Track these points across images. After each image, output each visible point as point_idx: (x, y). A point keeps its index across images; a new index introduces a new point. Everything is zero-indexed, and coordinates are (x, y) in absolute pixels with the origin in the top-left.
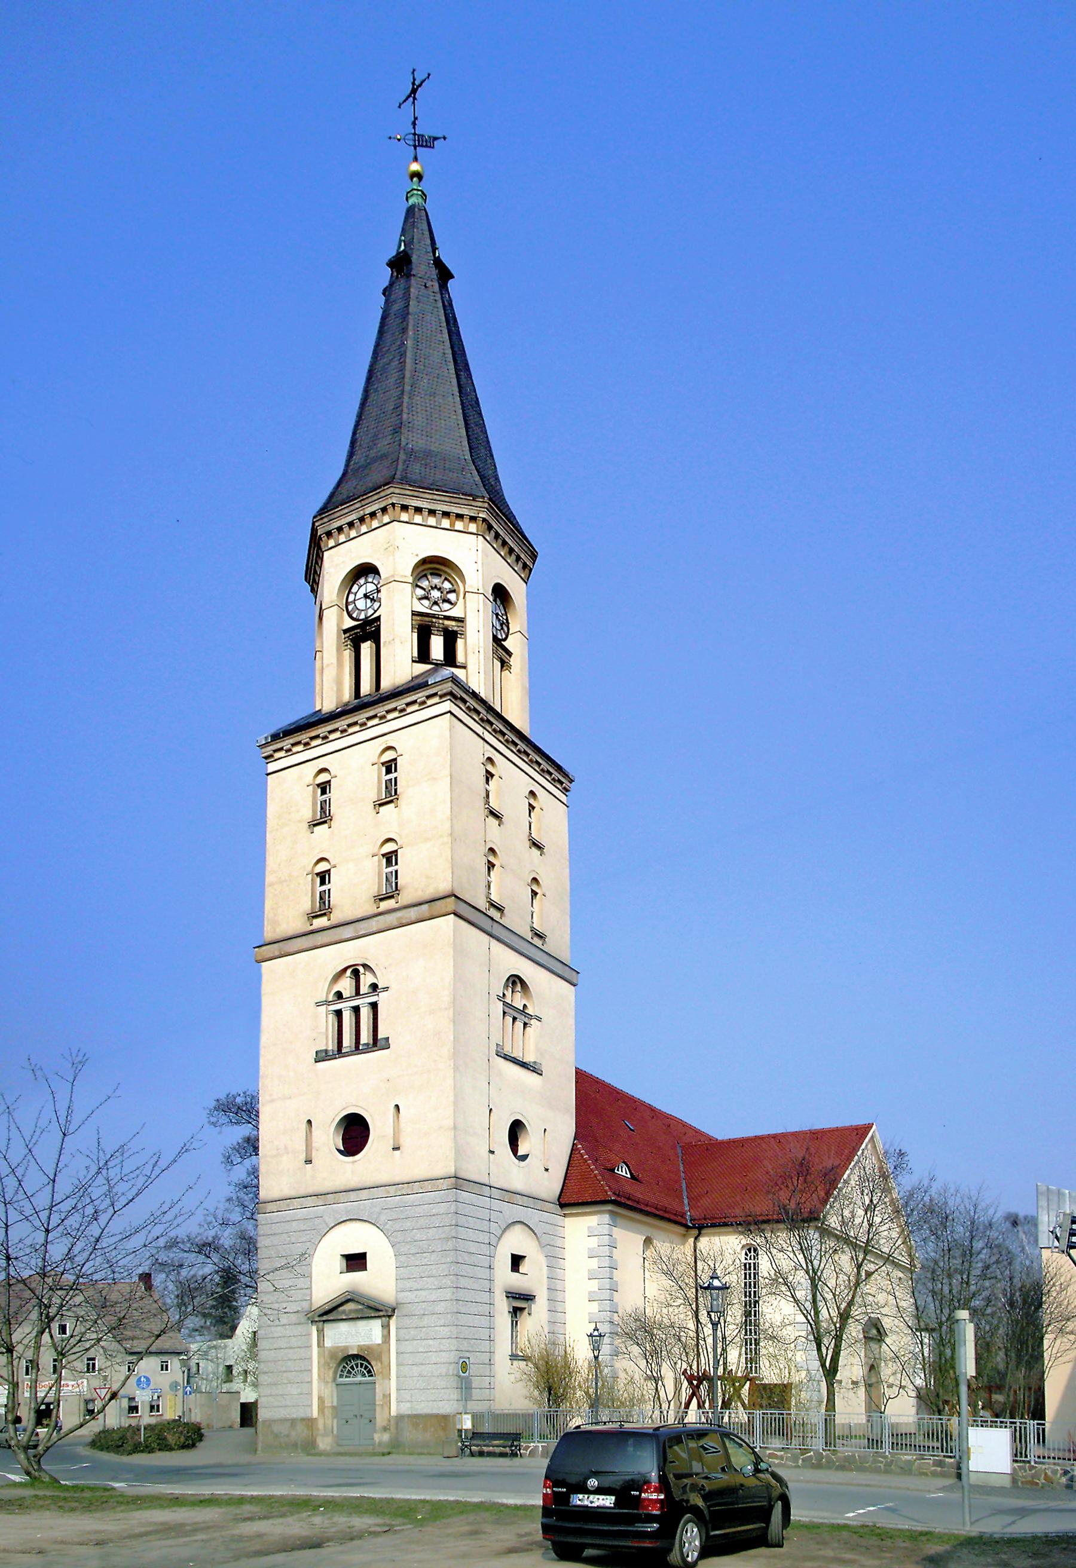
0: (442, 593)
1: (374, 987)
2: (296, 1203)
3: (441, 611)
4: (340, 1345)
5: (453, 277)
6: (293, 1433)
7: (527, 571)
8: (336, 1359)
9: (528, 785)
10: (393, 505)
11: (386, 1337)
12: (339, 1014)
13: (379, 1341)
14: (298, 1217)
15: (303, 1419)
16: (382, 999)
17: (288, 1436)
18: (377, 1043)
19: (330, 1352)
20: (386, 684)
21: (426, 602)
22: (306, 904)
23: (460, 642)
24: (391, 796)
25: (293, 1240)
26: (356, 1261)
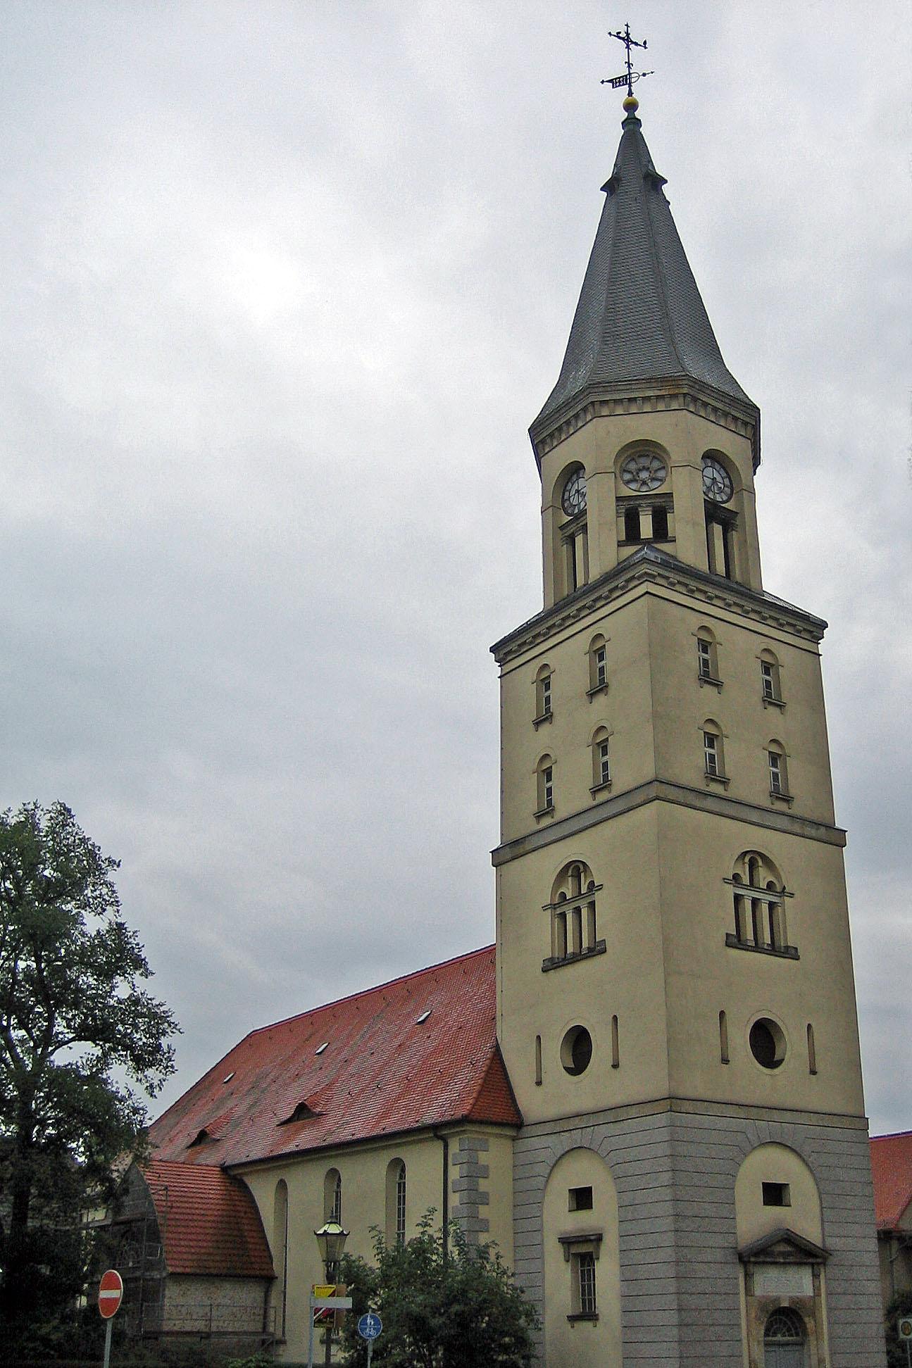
0: (650, 472)
2: (716, 1109)
5: (666, 182)
7: (749, 428)
11: (817, 1289)
16: (598, 896)
21: (633, 486)
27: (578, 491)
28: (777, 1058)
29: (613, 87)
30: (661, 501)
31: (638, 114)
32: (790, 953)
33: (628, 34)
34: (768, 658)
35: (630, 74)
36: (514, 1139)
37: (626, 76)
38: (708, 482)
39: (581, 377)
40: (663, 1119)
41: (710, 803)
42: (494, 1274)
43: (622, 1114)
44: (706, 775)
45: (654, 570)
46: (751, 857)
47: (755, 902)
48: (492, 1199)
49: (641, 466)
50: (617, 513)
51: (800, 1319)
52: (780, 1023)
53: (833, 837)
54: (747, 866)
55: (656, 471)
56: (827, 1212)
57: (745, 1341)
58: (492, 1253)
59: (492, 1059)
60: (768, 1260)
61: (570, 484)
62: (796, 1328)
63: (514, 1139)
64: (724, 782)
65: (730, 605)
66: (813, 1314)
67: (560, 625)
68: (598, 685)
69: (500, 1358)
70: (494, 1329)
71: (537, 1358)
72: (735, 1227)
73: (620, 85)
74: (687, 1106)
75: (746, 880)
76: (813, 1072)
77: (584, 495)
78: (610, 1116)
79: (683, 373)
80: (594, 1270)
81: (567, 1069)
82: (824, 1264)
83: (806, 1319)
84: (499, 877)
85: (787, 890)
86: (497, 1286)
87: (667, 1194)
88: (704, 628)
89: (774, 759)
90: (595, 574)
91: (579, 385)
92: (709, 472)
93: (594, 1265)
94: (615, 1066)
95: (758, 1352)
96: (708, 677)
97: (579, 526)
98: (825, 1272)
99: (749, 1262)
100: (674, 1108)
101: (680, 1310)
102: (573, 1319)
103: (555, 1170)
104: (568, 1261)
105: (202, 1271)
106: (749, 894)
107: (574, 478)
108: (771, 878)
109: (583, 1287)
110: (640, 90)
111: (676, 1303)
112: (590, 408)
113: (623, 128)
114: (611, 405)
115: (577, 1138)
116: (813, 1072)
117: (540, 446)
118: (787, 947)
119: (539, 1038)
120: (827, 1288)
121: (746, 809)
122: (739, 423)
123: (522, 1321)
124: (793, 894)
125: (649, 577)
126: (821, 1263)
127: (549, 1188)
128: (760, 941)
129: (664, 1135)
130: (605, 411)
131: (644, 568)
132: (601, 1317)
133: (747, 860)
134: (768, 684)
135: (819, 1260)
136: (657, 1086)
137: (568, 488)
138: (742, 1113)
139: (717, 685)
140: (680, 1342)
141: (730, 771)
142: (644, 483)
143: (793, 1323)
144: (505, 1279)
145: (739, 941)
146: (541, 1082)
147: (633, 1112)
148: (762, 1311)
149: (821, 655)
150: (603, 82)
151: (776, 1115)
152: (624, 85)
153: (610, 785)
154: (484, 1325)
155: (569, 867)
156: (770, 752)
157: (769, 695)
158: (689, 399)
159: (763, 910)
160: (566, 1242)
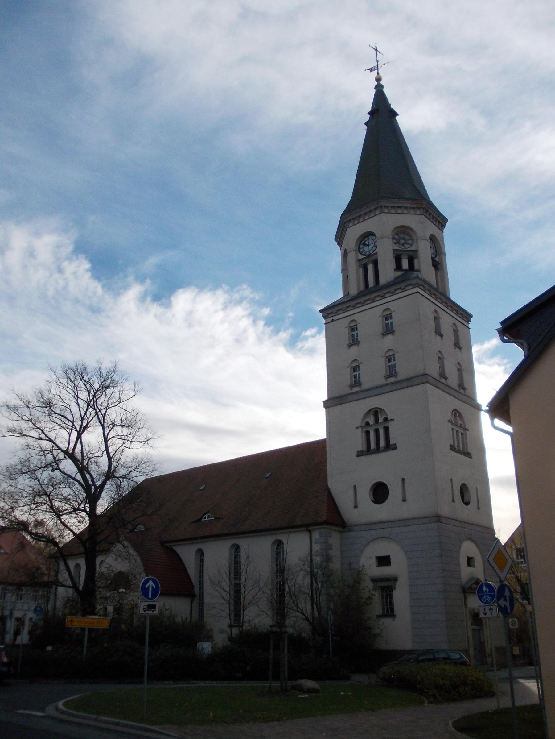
1: (386, 419)
3: (406, 248)
10: (381, 206)
12: (368, 433)
18: (389, 447)
20: (383, 280)
22: (348, 382)
23: (416, 261)
24: (389, 331)
26: (384, 561)
31: (382, 83)
36: (341, 532)
47: (457, 431)
64: (446, 378)
65: (443, 302)
96: (438, 332)
105: (314, 591)
112: (379, 208)
146: (357, 506)
149: (470, 329)
152: (375, 70)
153: (397, 375)
155: (463, 423)
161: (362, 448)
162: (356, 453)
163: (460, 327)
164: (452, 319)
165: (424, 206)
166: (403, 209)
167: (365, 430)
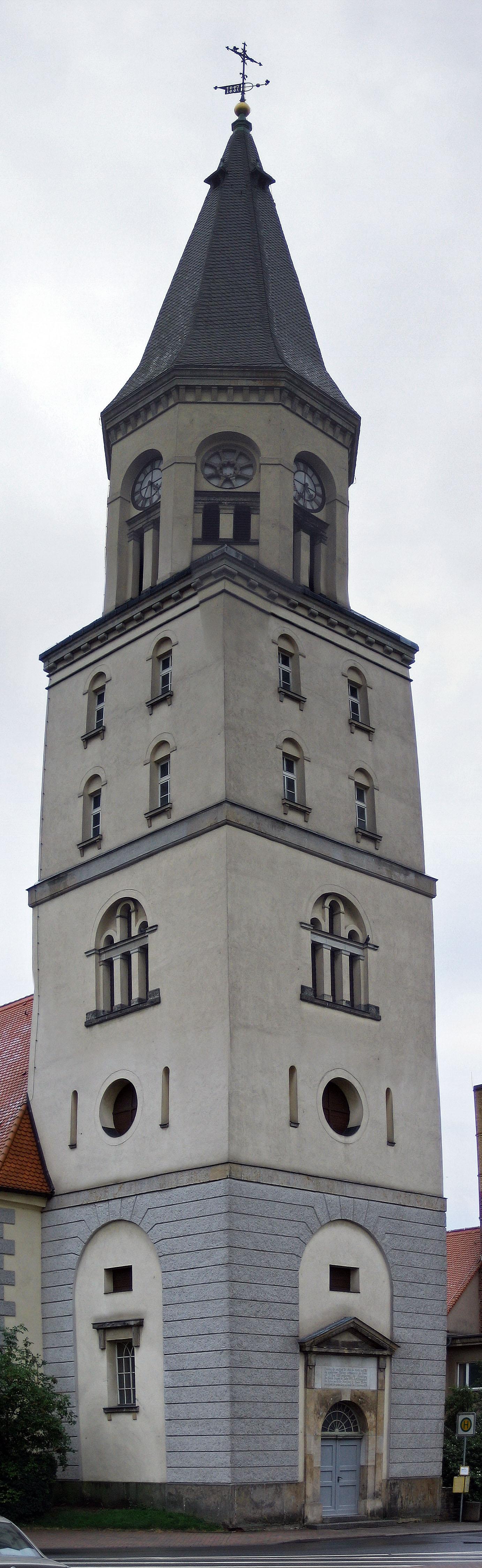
2: (282, 1178)
4: (332, 1387)
5: (273, 181)
6: (278, 1503)
7: (348, 437)
8: (327, 1407)
9: (346, 661)
10: (177, 387)
11: (380, 1382)
13: (374, 1388)
14: (283, 1199)
15: (289, 1483)
17: (271, 1505)
19: (319, 1394)
21: (215, 482)
25: (277, 1230)
27: (151, 484)
28: (351, 1124)
29: (226, 94)
30: (245, 500)
31: (249, 118)
32: (371, 1013)
33: (244, 51)
34: (355, 678)
35: (243, 84)
36: (43, 1211)
37: (240, 85)
38: (299, 487)
39: (166, 359)
40: (220, 1187)
41: (287, 834)
42: (24, 1362)
43: (172, 1181)
44: (285, 801)
45: (233, 568)
46: (333, 901)
47: (335, 953)
48: (18, 1278)
49: (225, 461)
50: (195, 508)
51: (361, 1414)
52: (356, 1085)
53: (423, 885)
54: (327, 911)
55: (242, 468)
56: (398, 1301)
57: (301, 1436)
58: (20, 1337)
59: (22, 1118)
60: (332, 1350)
61: (142, 476)
62: (355, 1423)
63: (43, 1211)
64: (305, 811)
66: (375, 1409)
67: (121, 628)
68: (160, 693)
69: (34, 1451)
70: (26, 1420)
71: (74, 1451)
72: (298, 1314)
73: (233, 92)
74: (248, 1173)
75: (325, 926)
76: (391, 1143)
77: (158, 488)
78: (155, 1184)
79: (282, 365)
80: (133, 1359)
81: (108, 1131)
82: (390, 1356)
83: (367, 1414)
84: (37, 918)
85: (370, 942)
86: (28, 1375)
87: (222, 1273)
88: (285, 637)
89: (361, 791)
90: (164, 573)
91: (164, 367)
92: (301, 476)
93: (133, 1354)
94: (164, 1126)
95: (315, 1447)
97: (150, 520)
98: (391, 1364)
99: (311, 1352)
100: (233, 1175)
101: (233, 1402)
102: (110, 1411)
103: (89, 1247)
104: (103, 1349)
106: (328, 943)
107: (148, 469)
108: (354, 927)
109: (121, 1376)
110: (252, 99)
111: (228, 1394)
112: (174, 393)
113: (232, 130)
114: (198, 391)
115: (116, 1209)
116: (391, 1143)
117: (113, 432)
118: (368, 1006)
119: (75, 1093)
120: (391, 1382)
121: (329, 845)
122: (338, 430)
123: (55, 1413)
124: (378, 947)
125: (227, 575)
126: (388, 1355)
127: (81, 1269)
128: (337, 998)
129: (221, 1205)
130: (190, 398)
131: (223, 564)
132: (141, 1409)
133: (327, 903)
134: (354, 707)
135: (386, 1353)
136: (216, 1151)
137: (141, 479)
138: (310, 1184)
139: (299, 700)
140: (232, 1435)
141: (311, 800)
142: (228, 480)
143: (353, 1418)
144: (35, 1367)
145: (315, 995)
147: (184, 1179)
148: (322, 1404)
149: (411, 681)
150: (216, 88)
151: (349, 1189)
152: (237, 92)
153: (171, 808)
154: (15, 1416)
156: (356, 783)
157: (355, 718)
158: (285, 394)
159: (343, 962)
160: (101, 1328)
161: (97, 1004)
162: (84, 1019)
163: (373, 675)
164: (348, 656)
165: (283, 384)
166: (231, 392)
167: (104, 957)
